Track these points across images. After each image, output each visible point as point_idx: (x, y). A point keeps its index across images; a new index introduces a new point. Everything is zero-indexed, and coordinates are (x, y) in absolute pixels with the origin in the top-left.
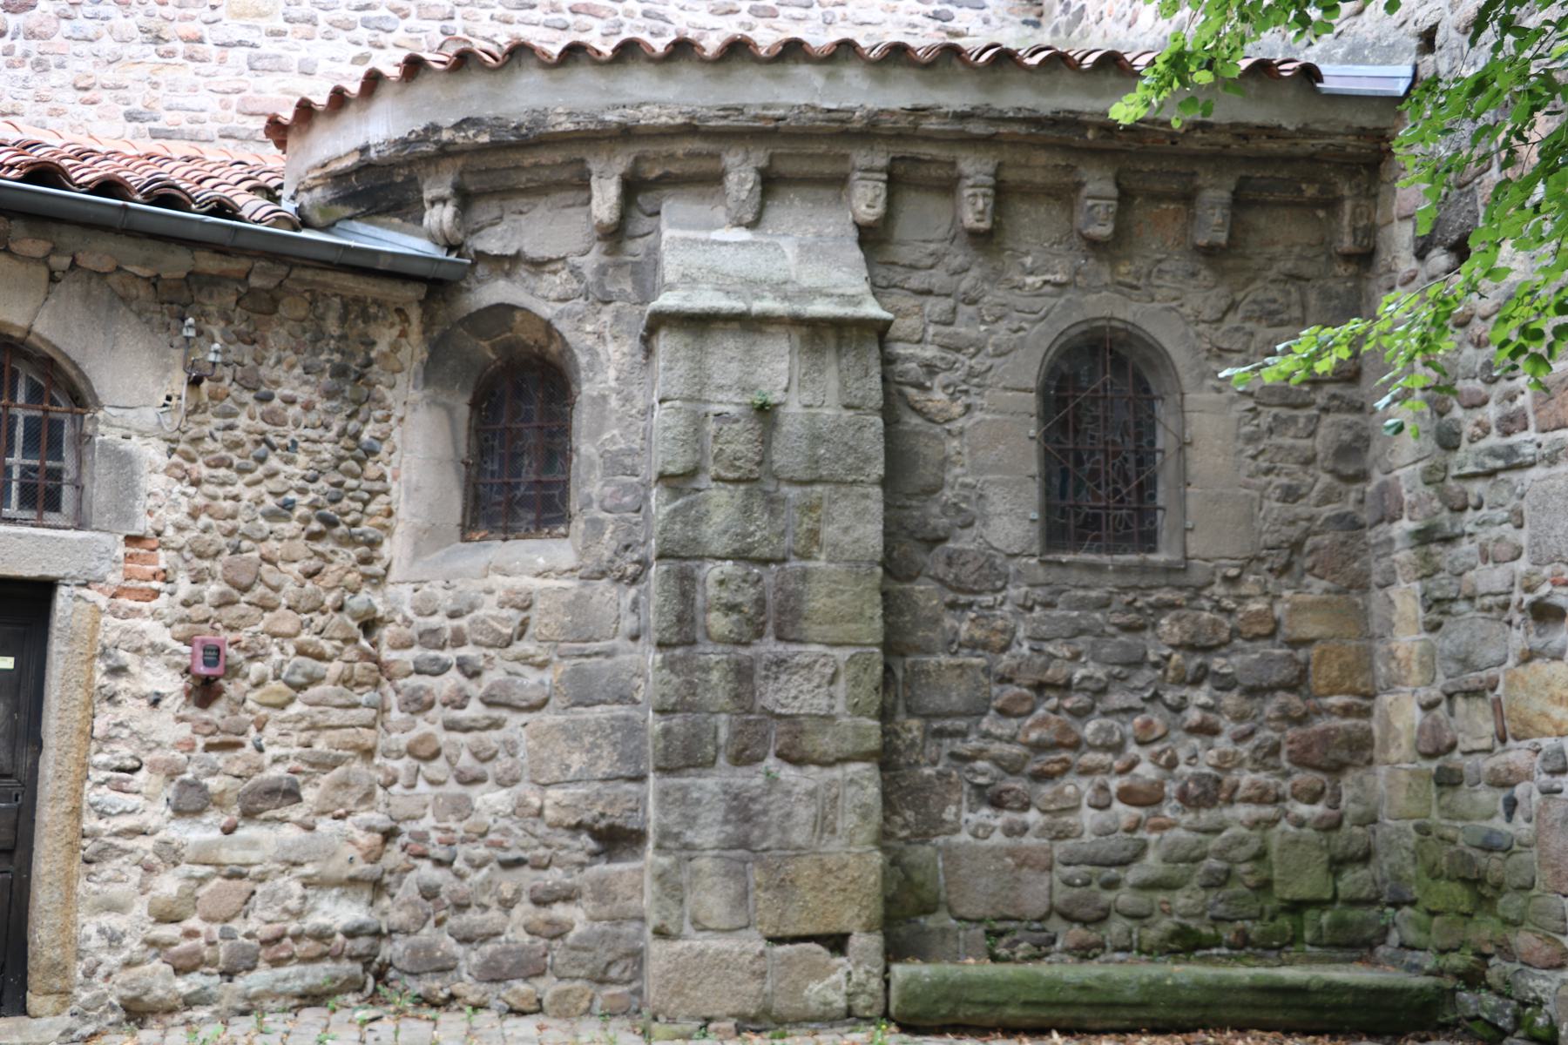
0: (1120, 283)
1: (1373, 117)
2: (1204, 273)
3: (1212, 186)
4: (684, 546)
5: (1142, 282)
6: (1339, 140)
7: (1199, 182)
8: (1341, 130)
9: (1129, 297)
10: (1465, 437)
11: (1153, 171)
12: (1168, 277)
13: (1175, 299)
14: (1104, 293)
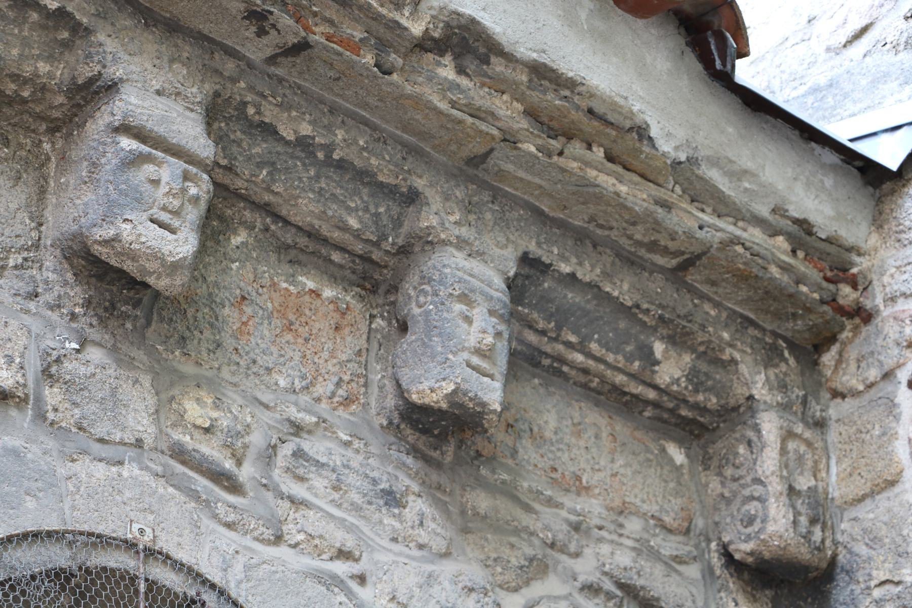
0: (180, 454)
1: (828, 211)
2: (417, 505)
3: (461, 244)
4: (84, 452)
5: (246, 473)
6: (755, 235)
7: (429, 219)
8: (764, 211)
9: (207, 504)
10: (888, 273)
11: (304, 144)
12: (319, 483)
13: (343, 554)
14: (130, 470)
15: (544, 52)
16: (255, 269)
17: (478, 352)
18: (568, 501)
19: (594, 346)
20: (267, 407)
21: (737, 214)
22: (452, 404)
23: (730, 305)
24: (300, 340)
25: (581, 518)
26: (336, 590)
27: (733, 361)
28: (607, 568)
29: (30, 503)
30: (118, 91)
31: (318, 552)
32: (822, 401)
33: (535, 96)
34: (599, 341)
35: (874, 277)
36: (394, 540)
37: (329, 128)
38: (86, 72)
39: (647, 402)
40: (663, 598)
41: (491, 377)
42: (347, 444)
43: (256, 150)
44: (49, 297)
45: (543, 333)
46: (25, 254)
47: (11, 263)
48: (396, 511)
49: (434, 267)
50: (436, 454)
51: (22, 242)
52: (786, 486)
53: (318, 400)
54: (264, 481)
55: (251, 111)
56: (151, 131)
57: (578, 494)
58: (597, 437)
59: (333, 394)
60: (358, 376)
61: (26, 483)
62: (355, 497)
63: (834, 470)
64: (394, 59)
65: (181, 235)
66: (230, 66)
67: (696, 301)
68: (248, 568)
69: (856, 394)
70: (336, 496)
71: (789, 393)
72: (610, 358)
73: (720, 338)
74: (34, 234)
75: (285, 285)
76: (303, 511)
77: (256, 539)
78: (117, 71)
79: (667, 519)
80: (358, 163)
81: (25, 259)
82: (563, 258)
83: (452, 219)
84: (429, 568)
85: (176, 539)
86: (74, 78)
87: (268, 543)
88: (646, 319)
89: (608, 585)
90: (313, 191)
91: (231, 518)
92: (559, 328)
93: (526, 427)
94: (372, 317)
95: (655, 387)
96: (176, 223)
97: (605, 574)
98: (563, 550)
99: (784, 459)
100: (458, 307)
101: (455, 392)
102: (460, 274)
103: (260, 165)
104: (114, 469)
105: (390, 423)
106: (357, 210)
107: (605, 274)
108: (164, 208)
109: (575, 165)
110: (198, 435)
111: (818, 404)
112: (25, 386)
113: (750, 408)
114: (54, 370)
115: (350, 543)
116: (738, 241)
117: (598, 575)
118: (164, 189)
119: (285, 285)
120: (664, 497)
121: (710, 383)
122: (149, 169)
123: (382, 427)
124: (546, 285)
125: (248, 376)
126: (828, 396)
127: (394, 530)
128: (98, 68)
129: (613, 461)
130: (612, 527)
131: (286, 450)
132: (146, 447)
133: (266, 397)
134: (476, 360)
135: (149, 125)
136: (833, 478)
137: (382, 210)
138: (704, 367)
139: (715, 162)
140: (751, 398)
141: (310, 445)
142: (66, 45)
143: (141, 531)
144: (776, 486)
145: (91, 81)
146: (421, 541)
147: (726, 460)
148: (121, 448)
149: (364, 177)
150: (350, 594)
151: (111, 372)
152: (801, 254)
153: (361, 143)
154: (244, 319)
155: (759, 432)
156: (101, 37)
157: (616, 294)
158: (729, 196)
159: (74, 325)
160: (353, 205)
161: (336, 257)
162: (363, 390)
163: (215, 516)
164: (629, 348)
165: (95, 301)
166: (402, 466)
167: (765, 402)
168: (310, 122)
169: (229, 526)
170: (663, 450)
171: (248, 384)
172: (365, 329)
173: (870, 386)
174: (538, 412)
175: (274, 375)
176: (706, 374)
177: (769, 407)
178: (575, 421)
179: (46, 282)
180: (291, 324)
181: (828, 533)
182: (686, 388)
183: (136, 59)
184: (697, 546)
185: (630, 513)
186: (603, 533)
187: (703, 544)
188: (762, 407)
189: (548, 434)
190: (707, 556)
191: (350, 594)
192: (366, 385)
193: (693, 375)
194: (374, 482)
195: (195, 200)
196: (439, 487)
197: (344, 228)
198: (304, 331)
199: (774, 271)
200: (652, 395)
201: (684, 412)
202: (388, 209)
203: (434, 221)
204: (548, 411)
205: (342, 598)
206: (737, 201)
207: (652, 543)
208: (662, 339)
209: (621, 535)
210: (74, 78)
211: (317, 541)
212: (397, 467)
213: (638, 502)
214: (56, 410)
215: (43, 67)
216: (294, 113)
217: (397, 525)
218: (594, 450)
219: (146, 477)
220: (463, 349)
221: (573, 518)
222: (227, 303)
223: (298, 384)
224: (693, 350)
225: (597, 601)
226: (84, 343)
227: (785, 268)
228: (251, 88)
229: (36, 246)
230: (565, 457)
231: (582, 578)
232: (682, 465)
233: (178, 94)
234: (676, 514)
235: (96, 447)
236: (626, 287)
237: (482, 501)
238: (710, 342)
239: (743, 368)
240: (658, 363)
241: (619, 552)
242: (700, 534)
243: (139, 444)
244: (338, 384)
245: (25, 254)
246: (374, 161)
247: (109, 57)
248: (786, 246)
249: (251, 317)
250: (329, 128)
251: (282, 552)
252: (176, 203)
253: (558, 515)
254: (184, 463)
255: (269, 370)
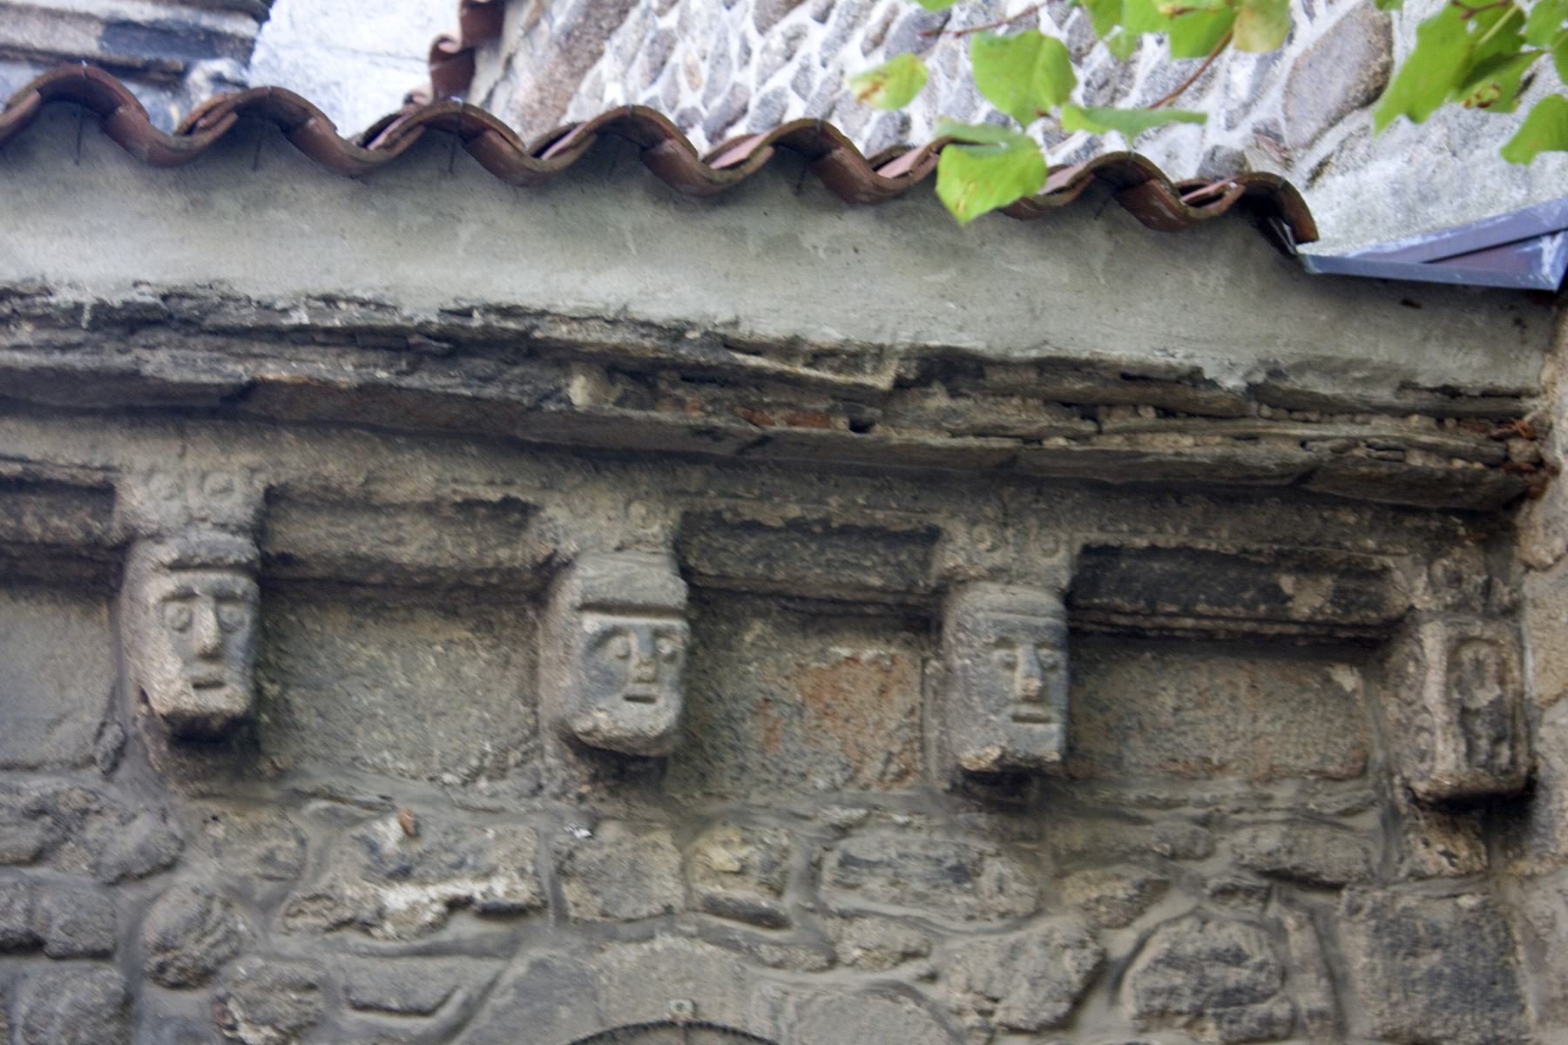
0: (714, 907)
2: (995, 868)
3: (995, 574)
8: (1383, 394)
11: (797, 527)
12: (875, 884)
13: (908, 956)
15: (1046, 342)
16: (777, 661)
17: (1027, 700)
18: (1193, 793)
19: (1201, 608)
20: (806, 818)
21: (1351, 411)
22: (1001, 767)
23: (1376, 500)
24: (840, 723)
25: (1211, 809)
26: (902, 998)
27: (1385, 569)
28: (1246, 861)
29: (564, 1012)
30: (574, 567)
31: (879, 963)
32: (1513, 578)
33: (1051, 389)
34: (1208, 602)
35: (1554, 419)
36: (970, 918)
37: (820, 501)
38: (544, 551)
39: (1295, 637)
40: (1326, 870)
41: (1045, 721)
42: (905, 826)
43: (746, 548)
44: (554, 787)
45: (1135, 613)
46: (524, 747)
47: (512, 761)
48: (968, 886)
49: (967, 613)
50: (1017, 799)
51: (518, 735)
52: (1457, 711)
53: (866, 787)
54: (810, 905)
55: (728, 516)
56: (614, 599)
57: (1209, 778)
58: (1233, 698)
59: (883, 774)
60: (910, 742)
61: (557, 993)
62: (919, 886)
63: (1530, 662)
64: (870, 412)
65: (661, 702)
66: (696, 477)
67: (1326, 514)
68: (799, 1007)
69: (1546, 568)
70: (896, 891)
71: (1464, 586)
72: (1227, 612)
73: (1365, 550)
74: (531, 721)
75: (814, 665)
76: (858, 923)
77: (810, 970)
78: (569, 546)
79: (1332, 768)
80: (860, 523)
81: (525, 753)
82: (1137, 532)
83: (982, 547)
84: (1012, 938)
85: (719, 999)
86: (534, 557)
87: (822, 969)
88: (1261, 560)
89: (1249, 880)
90: (820, 566)
91: (779, 955)
92: (1151, 604)
93: (1133, 722)
94: (925, 661)
95: (1296, 622)
96: (653, 690)
97: (1245, 866)
98: (1189, 855)
99: (1454, 676)
100: (999, 654)
101: (1002, 757)
102: (994, 616)
103: (753, 562)
104: (645, 946)
105: (954, 785)
106: (874, 566)
107: (1196, 531)
108: (640, 680)
109: (1118, 439)
110: (729, 880)
111: (1506, 584)
112: (542, 893)
113: (1414, 619)
114: (567, 867)
115: (913, 938)
116: (1354, 442)
117: (1234, 871)
118: (635, 661)
119: (814, 665)
120: (1328, 741)
121: (1363, 599)
122: (616, 644)
123: (946, 791)
124: (1123, 565)
125: (780, 789)
126: (1522, 569)
127: (968, 906)
128: (552, 546)
129: (1255, 719)
130: (1253, 805)
131: (831, 860)
132: (677, 911)
133: (802, 808)
134: (1025, 709)
135: (609, 596)
136: (1530, 674)
137: (903, 557)
138: (1351, 584)
139: (1301, 368)
140: (1412, 608)
141: (855, 846)
142: (521, 526)
143: (680, 1007)
144: (1440, 716)
145: (549, 559)
146: (1001, 909)
147: (1402, 675)
148: (649, 922)
149: (874, 534)
150: (918, 998)
151: (628, 846)
152: (1450, 423)
153: (861, 501)
154: (770, 724)
155: (1422, 648)
156: (551, 511)
157: (1213, 547)
158: (1335, 397)
159: (584, 807)
160: (868, 563)
161: (870, 610)
162: (919, 755)
163: (761, 962)
164: (1247, 596)
165: (601, 773)
166: (974, 829)
167: (1429, 611)
168: (797, 502)
169: (778, 965)
170: (1328, 680)
171: (780, 800)
172: (915, 679)
173: (1558, 559)
174: (1150, 695)
175: (811, 778)
176: (1356, 591)
177: (1433, 615)
178: (1202, 688)
179: (549, 770)
180: (828, 706)
181: (1521, 748)
182: (1334, 614)
183: (589, 520)
184: (1376, 787)
185: (1282, 777)
186: (1244, 817)
187: (1385, 782)
188: (1425, 617)
189: (1166, 718)
190: (1389, 795)
191: (918, 998)
192: (922, 749)
193: (1338, 597)
194: (939, 861)
195: (671, 658)
196: (1025, 837)
197: (867, 588)
198: (843, 711)
199: (1417, 460)
200: (1294, 630)
201: (1342, 634)
202: (911, 554)
203: (960, 560)
204: (1164, 689)
205: (910, 1005)
206: (1347, 398)
207: (1312, 806)
208: (1288, 571)
209: (1268, 810)
210: (534, 557)
211: (876, 954)
212: (968, 833)
213: (1291, 761)
214: (577, 905)
215: (503, 553)
216: (777, 500)
217: (971, 900)
218: (1230, 717)
219: (680, 943)
220: (1008, 702)
221: (1200, 812)
222: (748, 715)
223: (839, 778)
224: (1331, 570)
225: (1233, 903)
226: (594, 823)
227: (1428, 449)
228: (723, 494)
229: (535, 732)
230: (1188, 741)
231: (1213, 883)
232: (1354, 691)
233: (639, 541)
234: (1344, 757)
235: (624, 929)
236: (1225, 534)
237: (1077, 835)
238: (1349, 558)
239: (1398, 576)
240: (1290, 598)
241: (1263, 833)
242: (1381, 769)
243: (668, 910)
244: (888, 761)
245: (524, 747)
246: (880, 515)
247: (561, 531)
248: (1429, 422)
249: (777, 721)
250: (820, 501)
251: (840, 975)
252: (649, 671)
253: (1179, 816)
254: (719, 914)
255: (803, 776)
